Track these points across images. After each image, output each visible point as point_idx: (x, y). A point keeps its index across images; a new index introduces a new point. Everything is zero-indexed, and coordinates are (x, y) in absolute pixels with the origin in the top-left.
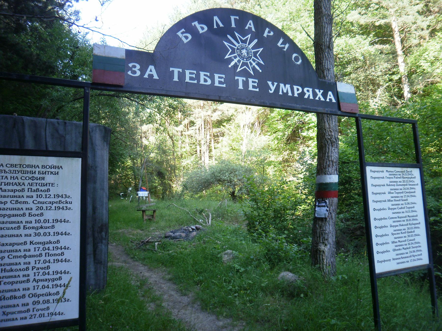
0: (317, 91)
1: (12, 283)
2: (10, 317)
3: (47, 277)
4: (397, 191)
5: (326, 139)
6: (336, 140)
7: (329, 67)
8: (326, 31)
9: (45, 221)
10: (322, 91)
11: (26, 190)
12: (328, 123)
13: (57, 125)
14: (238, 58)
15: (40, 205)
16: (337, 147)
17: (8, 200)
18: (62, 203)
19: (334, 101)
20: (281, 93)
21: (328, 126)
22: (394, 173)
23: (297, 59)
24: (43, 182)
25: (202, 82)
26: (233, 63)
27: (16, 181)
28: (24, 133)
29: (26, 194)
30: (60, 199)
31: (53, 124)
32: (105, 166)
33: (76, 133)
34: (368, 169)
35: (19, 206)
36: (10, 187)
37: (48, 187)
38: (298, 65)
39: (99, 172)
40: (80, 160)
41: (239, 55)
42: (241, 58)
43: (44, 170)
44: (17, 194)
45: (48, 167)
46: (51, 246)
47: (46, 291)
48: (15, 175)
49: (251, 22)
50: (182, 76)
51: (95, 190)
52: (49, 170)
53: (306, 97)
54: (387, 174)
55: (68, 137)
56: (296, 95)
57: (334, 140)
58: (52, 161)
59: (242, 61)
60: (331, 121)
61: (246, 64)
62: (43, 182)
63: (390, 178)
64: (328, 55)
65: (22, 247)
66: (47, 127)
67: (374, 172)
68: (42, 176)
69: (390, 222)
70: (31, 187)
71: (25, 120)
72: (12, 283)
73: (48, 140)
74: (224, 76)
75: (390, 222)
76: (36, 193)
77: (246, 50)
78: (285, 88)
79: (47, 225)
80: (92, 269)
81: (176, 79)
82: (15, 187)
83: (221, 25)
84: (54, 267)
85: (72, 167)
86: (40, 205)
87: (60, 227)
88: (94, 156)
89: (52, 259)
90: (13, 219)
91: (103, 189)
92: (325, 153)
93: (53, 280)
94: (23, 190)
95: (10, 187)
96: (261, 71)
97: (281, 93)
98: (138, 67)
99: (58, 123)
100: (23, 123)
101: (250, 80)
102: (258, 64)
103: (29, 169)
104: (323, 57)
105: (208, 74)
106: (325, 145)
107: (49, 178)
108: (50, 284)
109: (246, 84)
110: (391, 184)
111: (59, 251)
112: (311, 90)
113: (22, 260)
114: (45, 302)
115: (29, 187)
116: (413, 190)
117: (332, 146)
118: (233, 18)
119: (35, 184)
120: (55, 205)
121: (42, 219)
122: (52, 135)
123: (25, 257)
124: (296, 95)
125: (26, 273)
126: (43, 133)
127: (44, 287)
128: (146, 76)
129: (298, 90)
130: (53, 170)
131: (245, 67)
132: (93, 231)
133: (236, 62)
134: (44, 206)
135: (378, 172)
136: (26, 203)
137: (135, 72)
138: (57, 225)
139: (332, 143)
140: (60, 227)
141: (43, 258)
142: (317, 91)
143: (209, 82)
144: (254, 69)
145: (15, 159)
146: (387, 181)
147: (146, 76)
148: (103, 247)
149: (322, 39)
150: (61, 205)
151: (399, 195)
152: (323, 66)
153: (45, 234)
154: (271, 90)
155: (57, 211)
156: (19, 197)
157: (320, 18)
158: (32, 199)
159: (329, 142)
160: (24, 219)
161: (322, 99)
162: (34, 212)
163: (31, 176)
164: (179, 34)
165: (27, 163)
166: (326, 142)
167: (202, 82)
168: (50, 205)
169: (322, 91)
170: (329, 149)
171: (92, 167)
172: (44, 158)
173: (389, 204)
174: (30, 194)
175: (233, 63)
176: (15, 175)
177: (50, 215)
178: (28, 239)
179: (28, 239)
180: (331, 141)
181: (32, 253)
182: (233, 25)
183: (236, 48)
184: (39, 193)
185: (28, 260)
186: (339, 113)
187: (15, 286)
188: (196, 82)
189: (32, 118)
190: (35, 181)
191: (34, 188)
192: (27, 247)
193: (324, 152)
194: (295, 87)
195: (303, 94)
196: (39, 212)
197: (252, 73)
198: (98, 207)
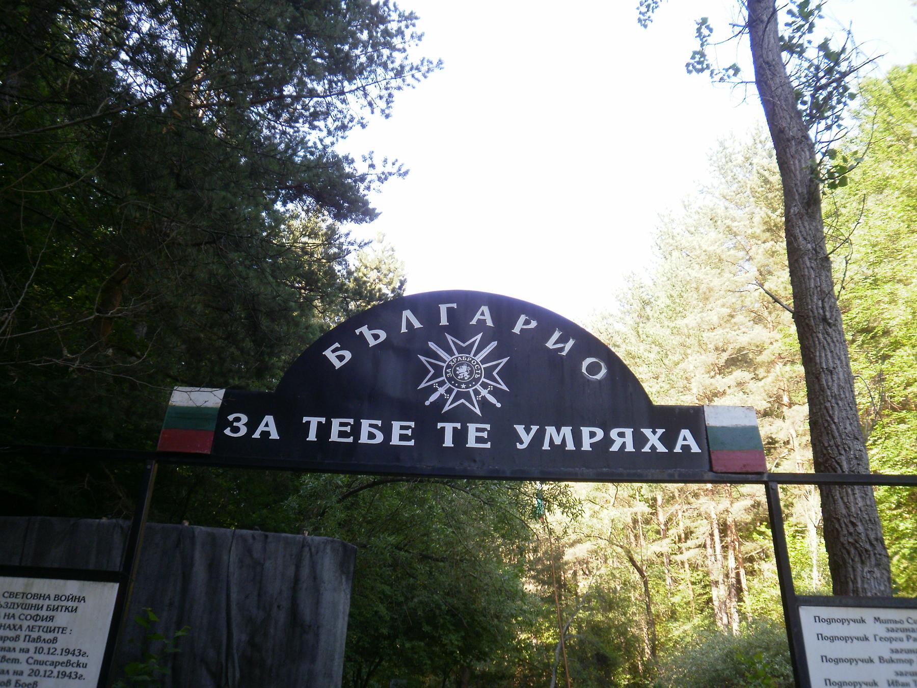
0: (647, 432)
5: (843, 544)
6: (871, 544)
7: (831, 365)
8: (812, 285)
10: (660, 432)
11: (22, 638)
12: (844, 503)
13: (250, 541)
15: (35, 667)
16: (878, 565)
20: (546, 446)
21: (844, 511)
22: (906, 625)
24: (50, 624)
25: (364, 439)
26: (433, 398)
27: (11, 621)
28: (192, 558)
29: (21, 644)
30: (70, 657)
31: (244, 539)
32: (340, 626)
33: (284, 556)
37: (55, 635)
38: (599, 382)
39: (323, 637)
40: (116, 586)
41: (450, 379)
42: (454, 385)
43: (56, 603)
44: (8, 644)
45: (63, 598)
48: (12, 611)
49: (485, 309)
50: (324, 430)
52: (64, 603)
53: (615, 448)
54: (881, 630)
55: (268, 564)
56: (586, 447)
57: (868, 547)
58: (72, 587)
59: (456, 390)
60: (852, 497)
61: (467, 396)
62: (50, 624)
63: (890, 640)
64: (825, 338)
66: (234, 545)
67: (830, 621)
68: (50, 613)
70: (31, 633)
71: (196, 533)
73: (231, 569)
74: (412, 424)
76: (35, 645)
77: (468, 365)
78: (558, 436)
81: (312, 436)
83: (417, 324)
86: (35, 667)
88: (317, 603)
92: (847, 583)
94: (16, 639)
96: (499, 405)
97: (546, 446)
98: (244, 419)
99: (254, 537)
100: (193, 538)
102: (495, 392)
103: (34, 602)
104: (815, 345)
105: (379, 423)
106: (845, 562)
107: (62, 619)
109: (460, 436)
110: (895, 656)
112: (629, 432)
115: (27, 633)
117: (863, 562)
118: (443, 308)
119: (37, 629)
120: (59, 668)
124: (586, 447)
126: (225, 558)
128: (257, 435)
129: (593, 435)
130: (70, 604)
131: (462, 401)
133: (486, 391)
134: (42, 668)
135: (842, 621)
136: (16, 661)
137: (236, 430)
139: (860, 556)
142: (647, 432)
143: (380, 438)
144: (484, 403)
145: (18, 584)
146: (884, 649)
147: (257, 435)
149: (807, 304)
150: (68, 670)
152: (816, 364)
154: (522, 443)
155: (60, 679)
156: (9, 650)
157: (797, 260)
158: (26, 656)
159: (853, 551)
161: (661, 448)
163: (33, 612)
165: (34, 592)
166: (844, 551)
167: (364, 439)
168: (52, 668)
169: (660, 432)
170: (854, 570)
171: (310, 626)
172: (60, 582)
175: (433, 398)
176: (12, 611)
180: (856, 548)
182: (444, 321)
183: (445, 365)
184: (39, 645)
186: (710, 475)
188: (351, 440)
189: (209, 529)
190: (40, 623)
191: (34, 635)
193: (843, 579)
194: (586, 431)
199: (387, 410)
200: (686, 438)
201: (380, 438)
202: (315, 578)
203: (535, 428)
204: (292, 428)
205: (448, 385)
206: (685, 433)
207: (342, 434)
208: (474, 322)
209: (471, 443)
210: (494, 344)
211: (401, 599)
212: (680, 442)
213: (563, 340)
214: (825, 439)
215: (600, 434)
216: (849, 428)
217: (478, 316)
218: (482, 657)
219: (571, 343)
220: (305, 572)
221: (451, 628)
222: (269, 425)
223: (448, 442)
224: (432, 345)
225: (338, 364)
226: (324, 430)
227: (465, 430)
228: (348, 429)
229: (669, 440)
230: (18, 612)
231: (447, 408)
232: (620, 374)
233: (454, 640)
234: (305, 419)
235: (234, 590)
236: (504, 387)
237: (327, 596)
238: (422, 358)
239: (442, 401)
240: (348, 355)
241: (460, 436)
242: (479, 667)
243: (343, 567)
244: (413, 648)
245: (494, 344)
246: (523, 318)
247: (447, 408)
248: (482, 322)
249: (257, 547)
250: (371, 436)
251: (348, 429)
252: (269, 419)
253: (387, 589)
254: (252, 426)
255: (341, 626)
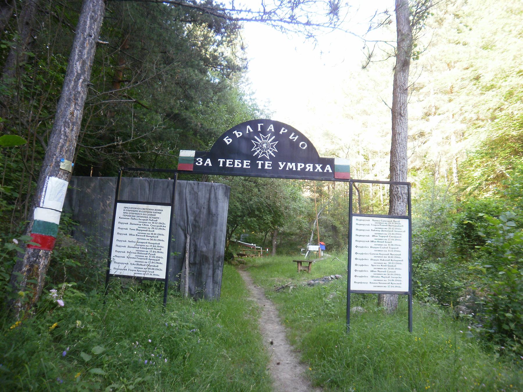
0: (317, 165)
1: (141, 259)
2: (140, 272)
3: (154, 258)
4: (382, 235)
7: (400, 131)
9: (155, 234)
10: (321, 165)
14: (260, 150)
17: (142, 224)
18: (161, 226)
19: (331, 171)
20: (287, 169)
23: (303, 145)
25: (236, 166)
26: (256, 153)
29: (148, 221)
31: (191, 185)
34: (354, 218)
35: (145, 226)
36: (143, 218)
39: (219, 218)
41: (261, 148)
44: (145, 221)
46: (156, 245)
47: (153, 264)
49: (272, 125)
50: (224, 163)
51: (216, 231)
53: (307, 170)
54: (374, 223)
55: (199, 193)
56: (299, 169)
58: (159, 207)
65: (145, 244)
69: (372, 257)
72: (141, 259)
74: (249, 161)
75: (372, 257)
78: (291, 166)
79: (155, 236)
80: (211, 287)
81: (221, 165)
82: (144, 218)
83: (251, 130)
84: (157, 255)
85: (167, 210)
87: (160, 237)
88: (217, 207)
89: (156, 251)
90: (143, 232)
91: (222, 231)
93: (156, 260)
95: (143, 218)
97: (287, 169)
98: (201, 160)
101: (267, 163)
102: (274, 152)
105: (240, 161)
108: (155, 262)
109: (263, 165)
111: (159, 248)
112: (312, 165)
113: (145, 250)
114: (152, 269)
116: (399, 236)
118: (259, 125)
121: (154, 233)
122: (190, 192)
123: (146, 248)
124: (299, 169)
125: (146, 255)
126: (185, 191)
127: (152, 263)
128: (205, 165)
129: (301, 166)
132: (213, 261)
137: (199, 163)
138: (159, 236)
140: (160, 237)
141: (153, 250)
144: (270, 155)
146: (373, 228)
147: (205, 165)
148: (219, 272)
151: (383, 238)
153: (154, 240)
160: (147, 232)
161: (321, 171)
162: (151, 230)
164: (225, 139)
167: (236, 166)
169: (321, 165)
173: (373, 244)
174: (150, 222)
175: (256, 153)
177: (157, 231)
178: (148, 241)
179: (148, 241)
181: (149, 247)
182: (259, 130)
185: (147, 250)
187: (142, 260)
188: (232, 166)
191: (151, 219)
192: (148, 244)
194: (299, 164)
195: (305, 168)
196: (153, 230)
197: (268, 158)
198: (218, 243)
199: (242, 157)
200: (328, 168)
201: (240, 166)
202: (216, 198)
203: (284, 163)
204: (215, 162)
205: (260, 150)
206: (328, 166)
207: (230, 164)
208: (268, 130)
209: (266, 167)
210: (274, 137)
211: (246, 200)
212: (326, 169)
213: (294, 136)
214: (394, 158)
215: (303, 165)
216: (402, 155)
217: (270, 128)
218: (281, 225)
219: (297, 137)
220: (213, 196)
221: (268, 213)
222: (209, 162)
223: (260, 167)
224: (256, 137)
225: (228, 143)
226: (224, 163)
227: (264, 163)
228: (231, 163)
229: (323, 168)
230: (146, 213)
231: (259, 157)
232: (311, 147)
233: (269, 218)
234: (219, 160)
235: (188, 202)
236: (276, 151)
237: (220, 205)
238: (253, 141)
239: (258, 154)
240: (231, 140)
241: (263, 165)
242: (281, 229)
243: (226, 194)
244: (251, 221)
245: (274, 137)
246: (283, 129)
247: (259, 157)
248: (270, 130)
249: (196, 187)
250: (238, 165)
251: (231, 163)
252: (209, 160)
253: (240, 195)
254: (204, 162)
255: (226, 214)
